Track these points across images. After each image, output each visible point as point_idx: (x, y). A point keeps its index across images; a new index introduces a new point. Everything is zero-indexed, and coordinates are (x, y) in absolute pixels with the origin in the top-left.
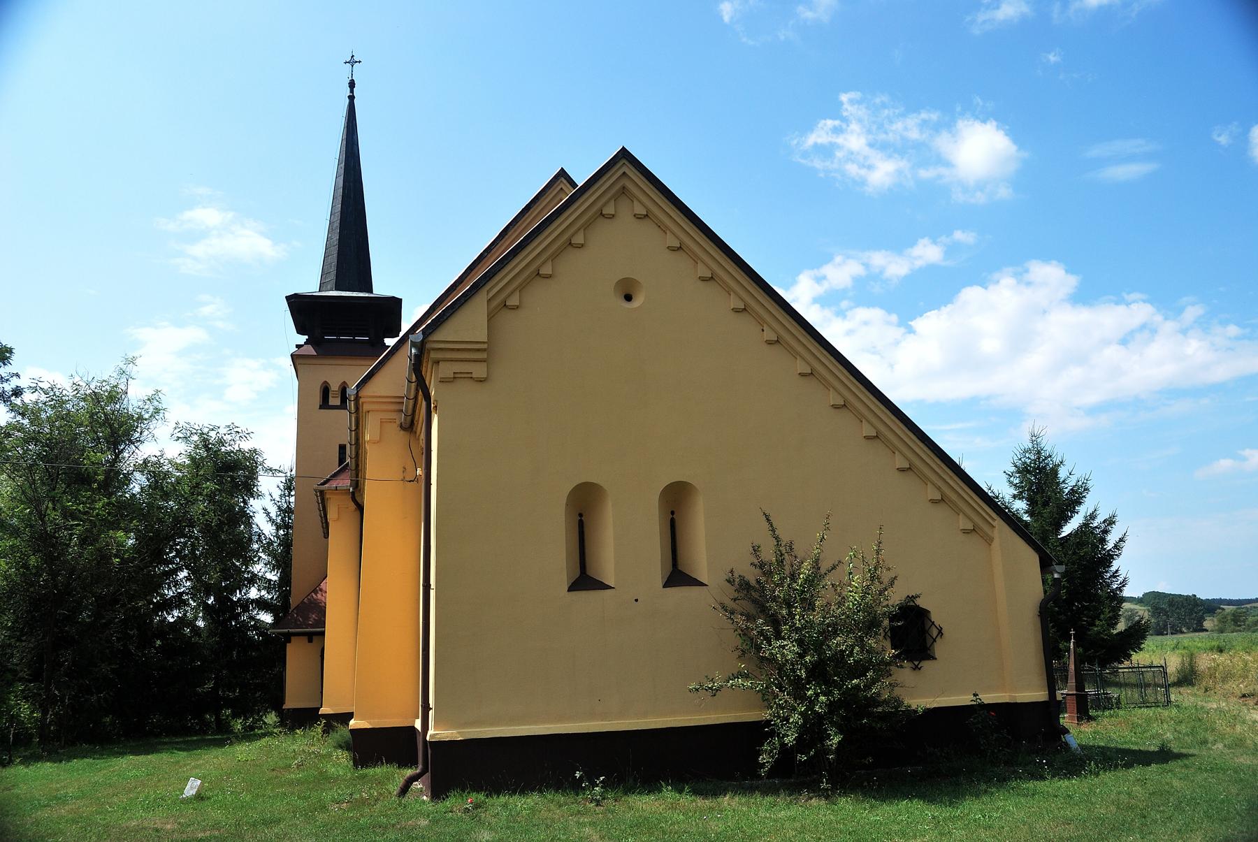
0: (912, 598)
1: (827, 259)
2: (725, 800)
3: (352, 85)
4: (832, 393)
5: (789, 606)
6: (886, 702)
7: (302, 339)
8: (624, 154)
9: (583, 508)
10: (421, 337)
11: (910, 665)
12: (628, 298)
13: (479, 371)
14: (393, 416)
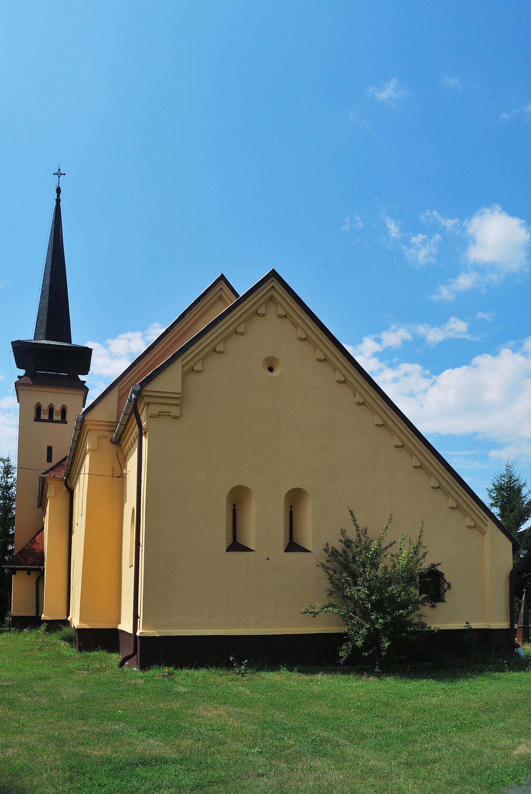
0: (433, 565)
1: (386, 328)
2: (319, 676)
3: (59, 191)
4: (395, 438)
5: (364, 566)
6: (416, 624)
7: (22, 372)
8: (273, 274)
9: (237, 502)
10: (139, 388)
11: (430, 604)
12: (271, 369)
13: (175, 411)
14: (106, 434)
